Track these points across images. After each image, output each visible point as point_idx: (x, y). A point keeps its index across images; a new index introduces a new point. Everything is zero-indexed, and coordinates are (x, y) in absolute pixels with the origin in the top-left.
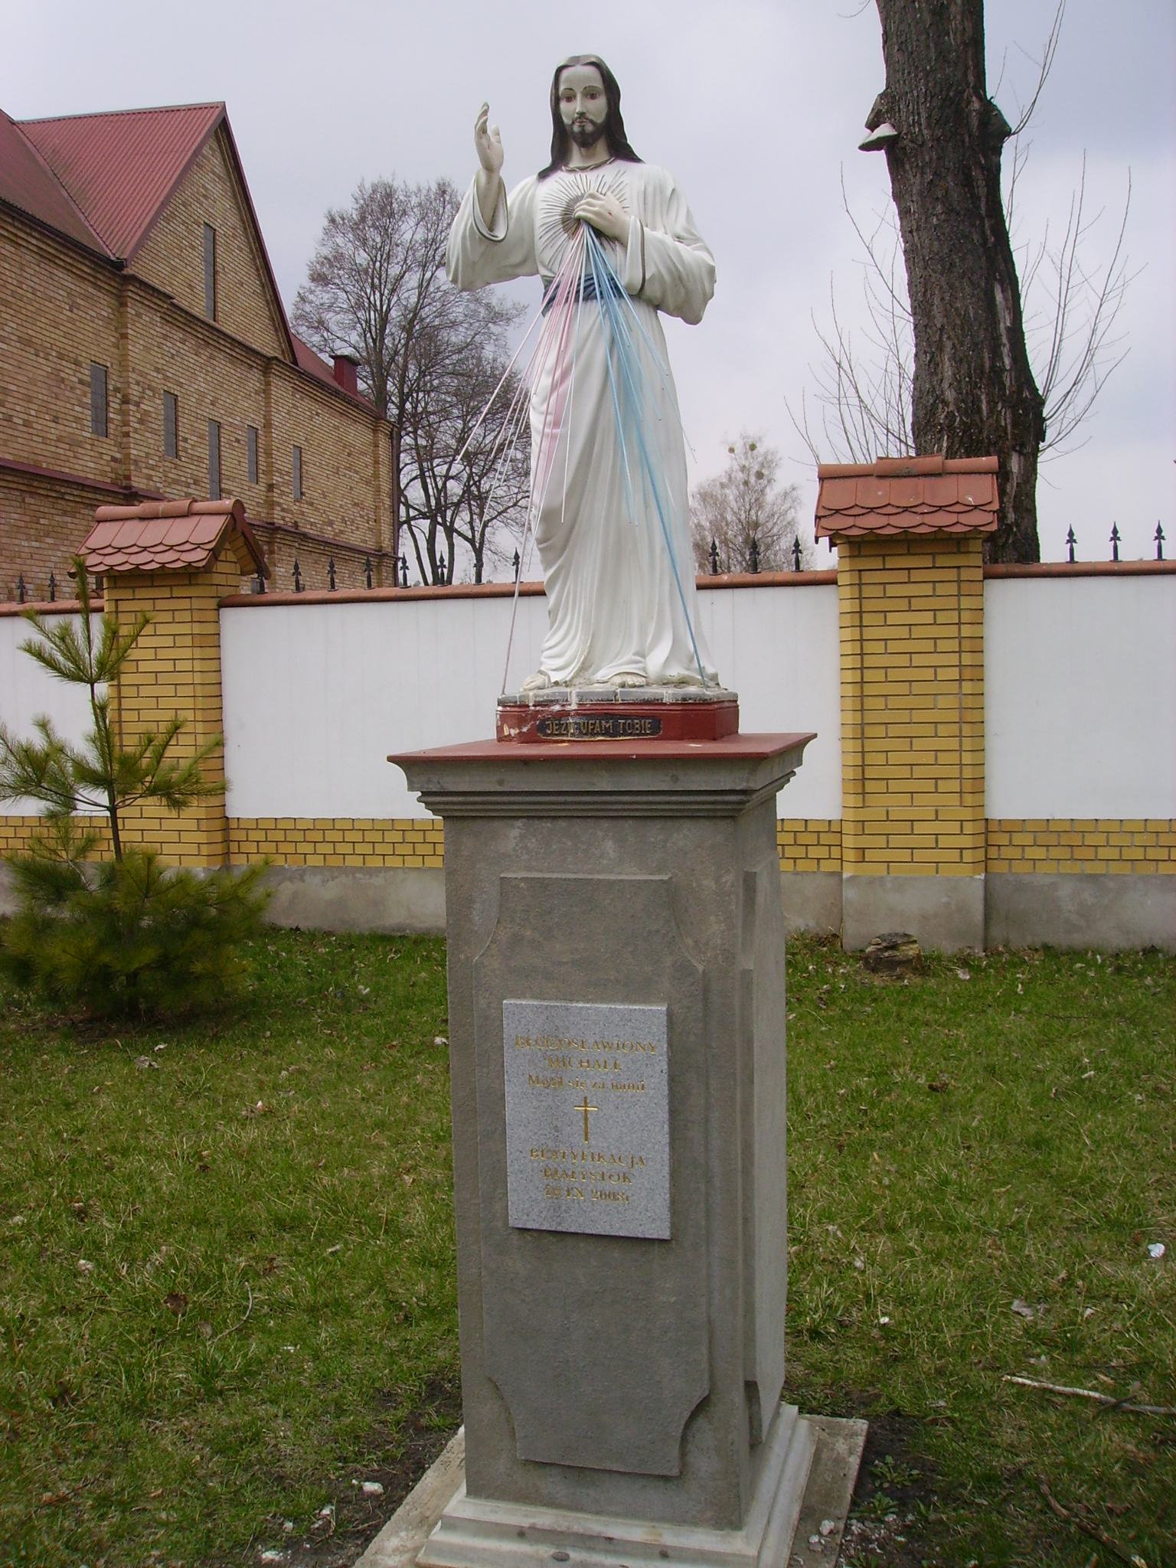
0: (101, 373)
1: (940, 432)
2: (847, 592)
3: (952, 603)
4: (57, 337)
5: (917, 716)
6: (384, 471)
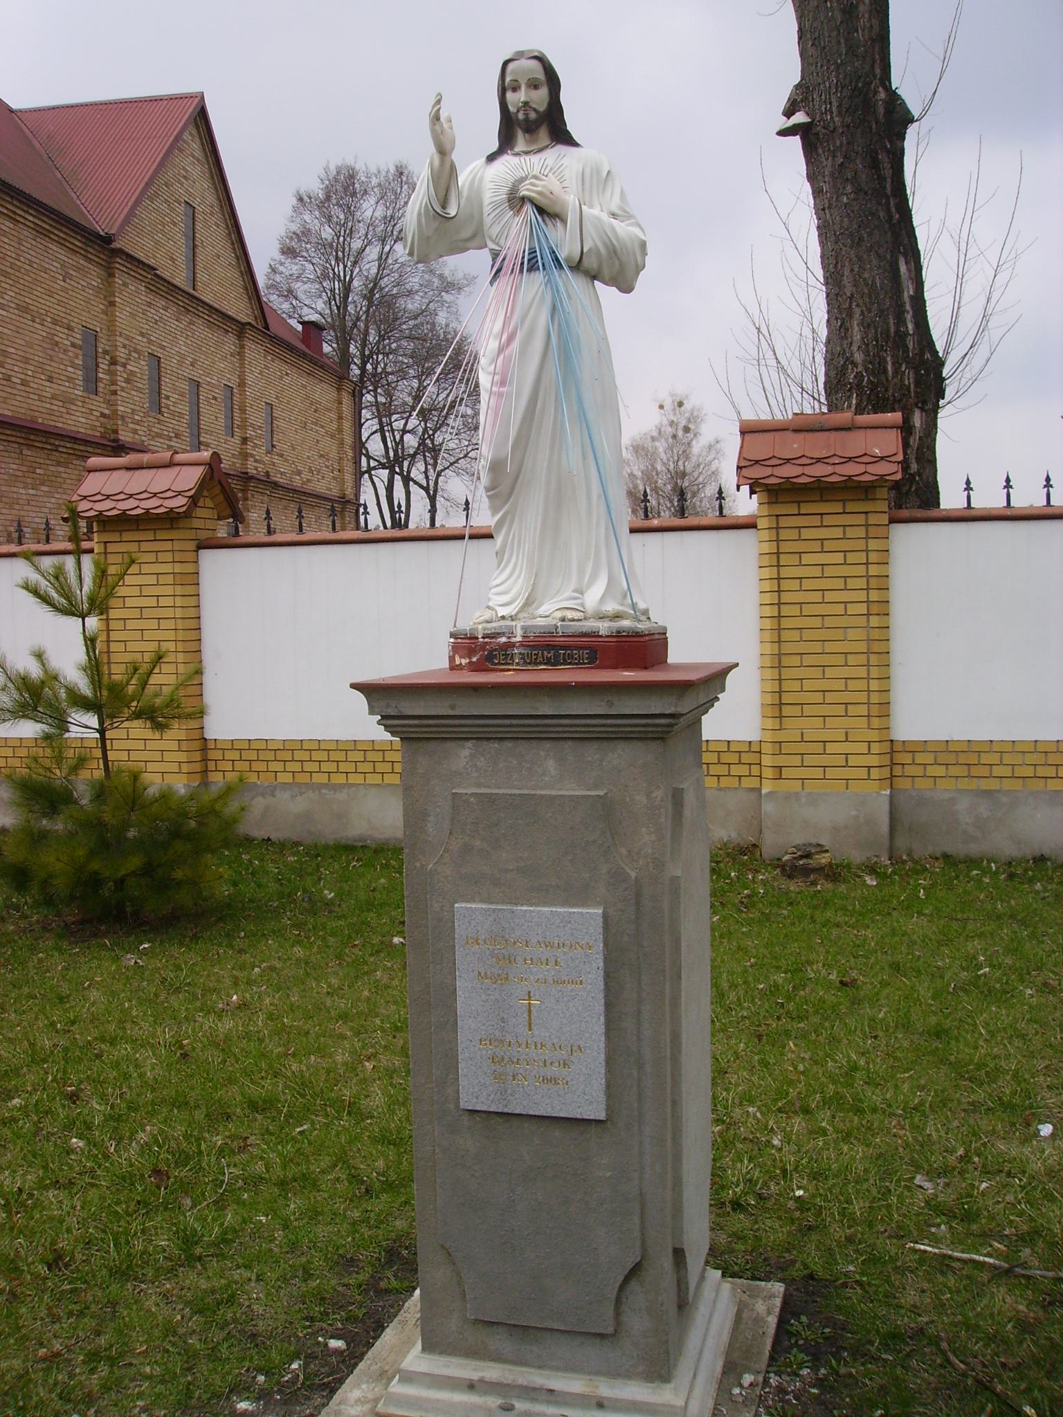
0: (91, 337)
1: (849, 390)
2: (765, 535)
3: (861, 545)
4: (51, 305)
5: (829, 647)
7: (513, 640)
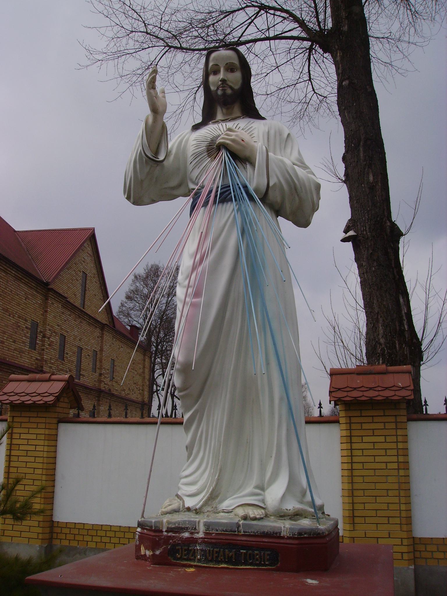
0: (35, 325)
1: (378, 356)
2: (344, 426)
3: (393, 432)
4: (18, 309)
5: (378, 486)
6: (147, 371)
7: (196, 536)
